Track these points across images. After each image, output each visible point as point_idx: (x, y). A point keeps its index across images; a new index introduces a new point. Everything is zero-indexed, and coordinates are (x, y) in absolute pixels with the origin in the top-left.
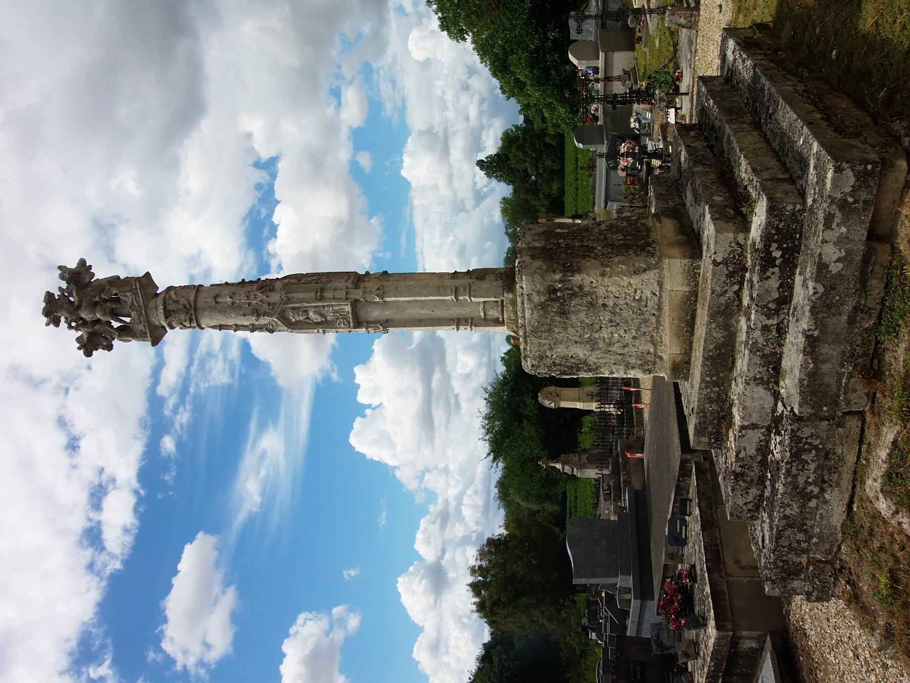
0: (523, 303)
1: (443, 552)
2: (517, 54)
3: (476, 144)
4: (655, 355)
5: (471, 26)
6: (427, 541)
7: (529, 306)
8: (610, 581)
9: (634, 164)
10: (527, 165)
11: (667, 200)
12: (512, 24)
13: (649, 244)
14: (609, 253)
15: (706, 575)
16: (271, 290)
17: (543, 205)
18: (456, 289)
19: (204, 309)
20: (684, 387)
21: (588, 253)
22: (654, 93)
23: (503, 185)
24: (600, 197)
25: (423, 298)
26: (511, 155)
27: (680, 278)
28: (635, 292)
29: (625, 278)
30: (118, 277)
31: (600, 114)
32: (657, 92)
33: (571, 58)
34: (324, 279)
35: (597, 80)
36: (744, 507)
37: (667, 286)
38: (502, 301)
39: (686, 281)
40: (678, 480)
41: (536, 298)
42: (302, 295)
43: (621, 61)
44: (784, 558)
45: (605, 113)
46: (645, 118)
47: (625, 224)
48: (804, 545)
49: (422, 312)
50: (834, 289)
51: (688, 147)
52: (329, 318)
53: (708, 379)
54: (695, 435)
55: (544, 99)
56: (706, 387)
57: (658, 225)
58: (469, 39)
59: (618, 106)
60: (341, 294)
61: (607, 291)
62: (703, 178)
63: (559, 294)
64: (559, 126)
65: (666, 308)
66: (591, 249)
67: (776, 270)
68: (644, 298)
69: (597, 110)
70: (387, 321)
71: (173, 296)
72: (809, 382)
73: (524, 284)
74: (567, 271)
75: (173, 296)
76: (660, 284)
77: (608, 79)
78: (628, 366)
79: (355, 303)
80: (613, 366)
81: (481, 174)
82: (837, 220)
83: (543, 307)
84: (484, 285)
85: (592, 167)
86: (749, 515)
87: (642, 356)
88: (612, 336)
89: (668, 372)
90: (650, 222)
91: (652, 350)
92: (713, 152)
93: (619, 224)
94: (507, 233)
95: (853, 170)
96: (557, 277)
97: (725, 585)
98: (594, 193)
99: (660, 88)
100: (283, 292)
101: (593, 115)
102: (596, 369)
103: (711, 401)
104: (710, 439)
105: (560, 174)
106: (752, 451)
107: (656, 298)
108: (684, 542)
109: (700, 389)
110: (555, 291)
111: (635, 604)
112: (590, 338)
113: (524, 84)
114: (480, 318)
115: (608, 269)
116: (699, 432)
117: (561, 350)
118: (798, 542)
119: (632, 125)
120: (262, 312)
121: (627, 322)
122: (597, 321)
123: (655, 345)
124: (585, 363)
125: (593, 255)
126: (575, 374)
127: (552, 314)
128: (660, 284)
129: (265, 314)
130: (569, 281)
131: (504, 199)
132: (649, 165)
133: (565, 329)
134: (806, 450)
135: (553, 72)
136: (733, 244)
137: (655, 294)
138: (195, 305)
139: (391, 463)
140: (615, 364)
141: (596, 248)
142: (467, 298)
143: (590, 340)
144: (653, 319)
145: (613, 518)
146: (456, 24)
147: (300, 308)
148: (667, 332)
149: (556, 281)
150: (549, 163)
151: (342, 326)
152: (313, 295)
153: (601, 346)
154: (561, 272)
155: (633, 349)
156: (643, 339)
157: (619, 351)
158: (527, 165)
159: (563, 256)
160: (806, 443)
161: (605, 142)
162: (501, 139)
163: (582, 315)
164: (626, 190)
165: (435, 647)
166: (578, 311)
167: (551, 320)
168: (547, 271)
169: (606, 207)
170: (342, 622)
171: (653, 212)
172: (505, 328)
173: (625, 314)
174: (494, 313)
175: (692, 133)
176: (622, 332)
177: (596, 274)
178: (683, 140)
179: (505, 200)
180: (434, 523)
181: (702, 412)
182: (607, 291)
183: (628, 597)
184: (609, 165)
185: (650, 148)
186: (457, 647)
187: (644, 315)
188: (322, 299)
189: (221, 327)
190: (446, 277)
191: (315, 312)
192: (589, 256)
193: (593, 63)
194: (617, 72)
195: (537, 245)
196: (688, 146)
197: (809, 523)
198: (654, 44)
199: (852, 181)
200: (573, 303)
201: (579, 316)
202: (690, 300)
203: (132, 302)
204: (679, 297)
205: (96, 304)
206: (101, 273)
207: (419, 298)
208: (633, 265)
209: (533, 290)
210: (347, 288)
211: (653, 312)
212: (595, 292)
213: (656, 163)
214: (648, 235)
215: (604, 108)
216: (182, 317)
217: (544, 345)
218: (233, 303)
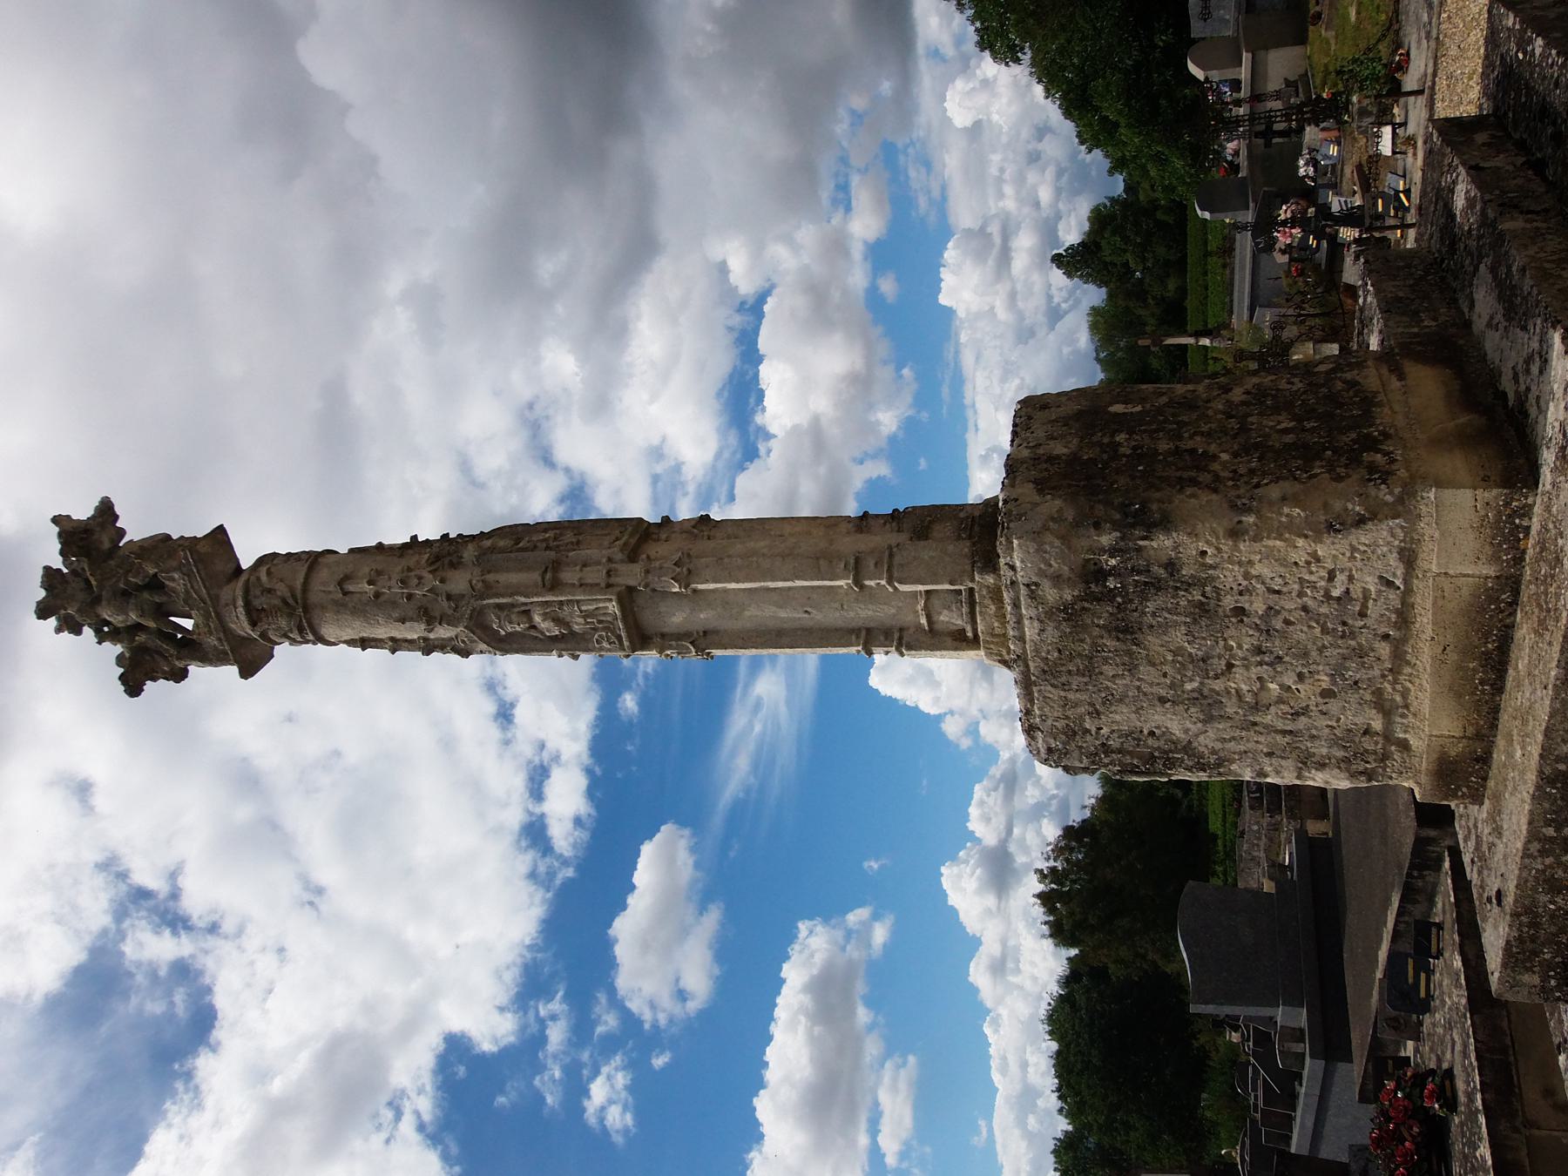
0: (1016, 605)
1: (1009, 831)
2: (1104, 78)
3: (1049, 230)
4: (1388, 736)
5: (1026, 35)
6: (987, 819)
7: (1033, 612)
8: (1266, 1012)
9: (1304, 239)
10: (1129, 256)
11: (1416, 313)
12: (1095, 28)
13: (1371, 444)
14: (1252, 472)
15: (1482, 1120)
16: (454, 566)
17: (1153, 315)
18: (857, 561)
19: (323, 608)
20: (1470, 818)
21: (1192, 471)
22: (1348, 101)
23: (1091, 287)
24: (1241, 301)
25: (780, 584)
26: (1103, 243)
27: (1469, 542)
28: (1331, 576)
29: (1300, 542)
30: (168, 537)
31: (1243, 160)
32: (1355, 99)
33: (1193, 68)
34: (569, 537)
35: (1238, 103)
37: (1430, 561)
38: (971, 590)
39: (1488, 550)
40: (1409, 875)
41: (1050, 594)
42: (514, 578)
43: (1281, 64)
45: (1250, 156)
46: (1326, 157)
47: (1299, 385)
49: (783, 614)
51: (1475, 170)
52: (576, 628)
53: (1550, 832)
54: (1505, 965)
55: (1149, 147)
56: (1543, 853)
57: (1395, 384)
58: (1027, 57)
59: (1275, 145)
60: (595, 575)
61: (1247, 576)
62: (1532, 251)
63: (1111, 583)
64: (1173, 189)
65: (1424, 621)
66: (1201, 461)
68: (1356, 592)
69: (1236, 153)
70: (705, 633)
71: (264, 578)
73: (1017, 557)
74: (1133, 526)
75: (264, 578)
76: (1409, 558)
77: (1256, 97)
78: (1306, 761)
79: (628, 598)
80: (1266, 760)
81: (1057, 276)
83: (1069, 614)
84: (926, 551)
85: (1228, 250)
87: (1345, 739)
88: (1263, 688)
89: (1424, 779)
90: (1371, 378)
91: (1377, 725)
92: (1544, 179)
93: (1283, 385)
94: (1097, 359)
96: (1106, 540)
97: (1524, 1152)
98: (1231, 294)
99: (1361, 89)
100: (477, 571)
101: (1231, 163)
102: (1219, 765)
105: (1181, 265)
107: (1394, 598)
108: (1425, 1006)
109: (1526, 854)
110: (1101, 575)
111: (1311, 1068)
112: (1199, 691)
113: (1116, 125)
114: (919, 627)
115: (1251, 519)
116: (1516, 956)
117: (1122, 718)
119: (1302, 172)
120: (437, 614)
121: (1306, 655)
122: (1219, 649)
124: (1188, 748)
125: (1205, 478)
126: (1162, 774)
127: (1096, 632)
128: (1409, 558)
129: (443, 619)
130: (1139, 550)
131: (1093, 308)
132: (1333, 239)
133: (1132, 669)
135: (1163, 102)
137: (1390, 584)
138: (305, 599)
139: (927, 706)
140: (1270, 755)
141: (1215, 457)
142: (883, 582)
143: (1199, 697)
144: (1384, 649)
145: (1268, 887)
146: (1002, 34)
147: (513, 605)
148: (1426, 681)
149: (1103, 551)
150: (1161, 251)
151: (605, 644)
152: (535, 576)
153: (1230, 710)
154: (1116, 526)
155: (1323, 722)
156: (1353, 698)
157: (1280, 725)
158: (1129, 256)
159: (1123, 481)
161: (1251, 205)
162: (1089, 219)
163: (1178, 637)
164: (1289, 285)
165: (998, 968)
166: (1165, 627)
167: (1094, 644)
168: (1077, 524)
169: (1251, 318)
170: (865, 931)
171: (1374, 343)
172: (982, 653)
173: (1300, 634)
174: (951, 618)
175: (1481, 138)
176: (1289, 679)
177: (1214, 532)
178: (1459, 153)
179: (1095, 311)
180: (995, 789)
181: (1526, 914)
182: (1247, 576)
183: (1298, 1048)
184: (1257, 244)
185: (1335, 208)
186: (1033, 964)
187: (1359, 642)
188: (555, 586)
189: (364, 643)
190: (844, 527)
191: (545, 616)
192: (1194, 482)
193: (1230, 74)
194: (1274, 84)
195: (1059, 449)
196: (1471, 168)
198: (1346, 17)
200: (1151, 606)
201: (1174, 639)
202: (1497, 601)
203: (187, 592)
204: (1465, 592)
205: (126, 594)
206: (136, 526)
207: (771, 585)
208: (1326, 506)
209: (1041, 573)
210: (610, 560)
211: (1383, 630)
212: (1213, 579)
213: (1347, 234)
214: (1367, 416)
215: (1249, 147)
216: (283, 623)
217: (1076, 705)
218: (377, 595)
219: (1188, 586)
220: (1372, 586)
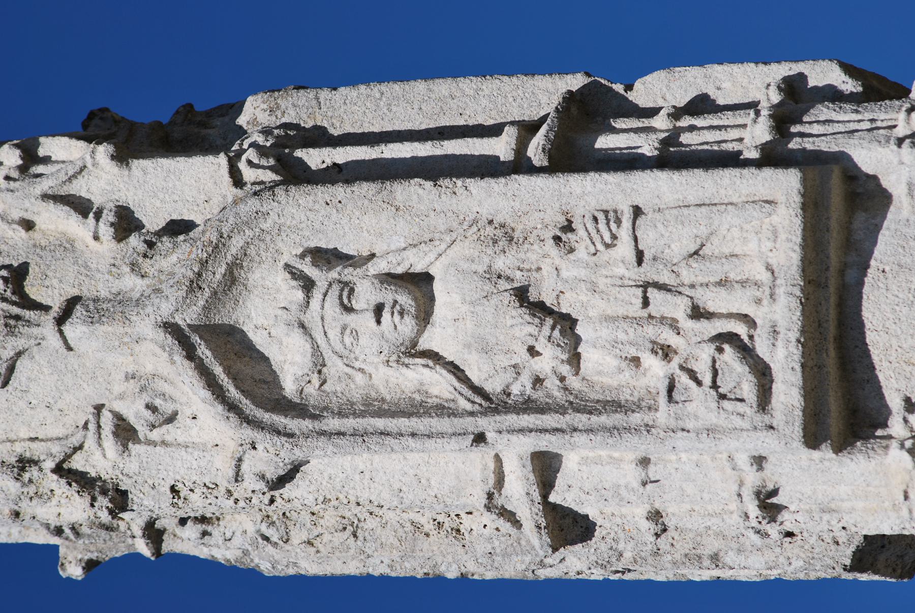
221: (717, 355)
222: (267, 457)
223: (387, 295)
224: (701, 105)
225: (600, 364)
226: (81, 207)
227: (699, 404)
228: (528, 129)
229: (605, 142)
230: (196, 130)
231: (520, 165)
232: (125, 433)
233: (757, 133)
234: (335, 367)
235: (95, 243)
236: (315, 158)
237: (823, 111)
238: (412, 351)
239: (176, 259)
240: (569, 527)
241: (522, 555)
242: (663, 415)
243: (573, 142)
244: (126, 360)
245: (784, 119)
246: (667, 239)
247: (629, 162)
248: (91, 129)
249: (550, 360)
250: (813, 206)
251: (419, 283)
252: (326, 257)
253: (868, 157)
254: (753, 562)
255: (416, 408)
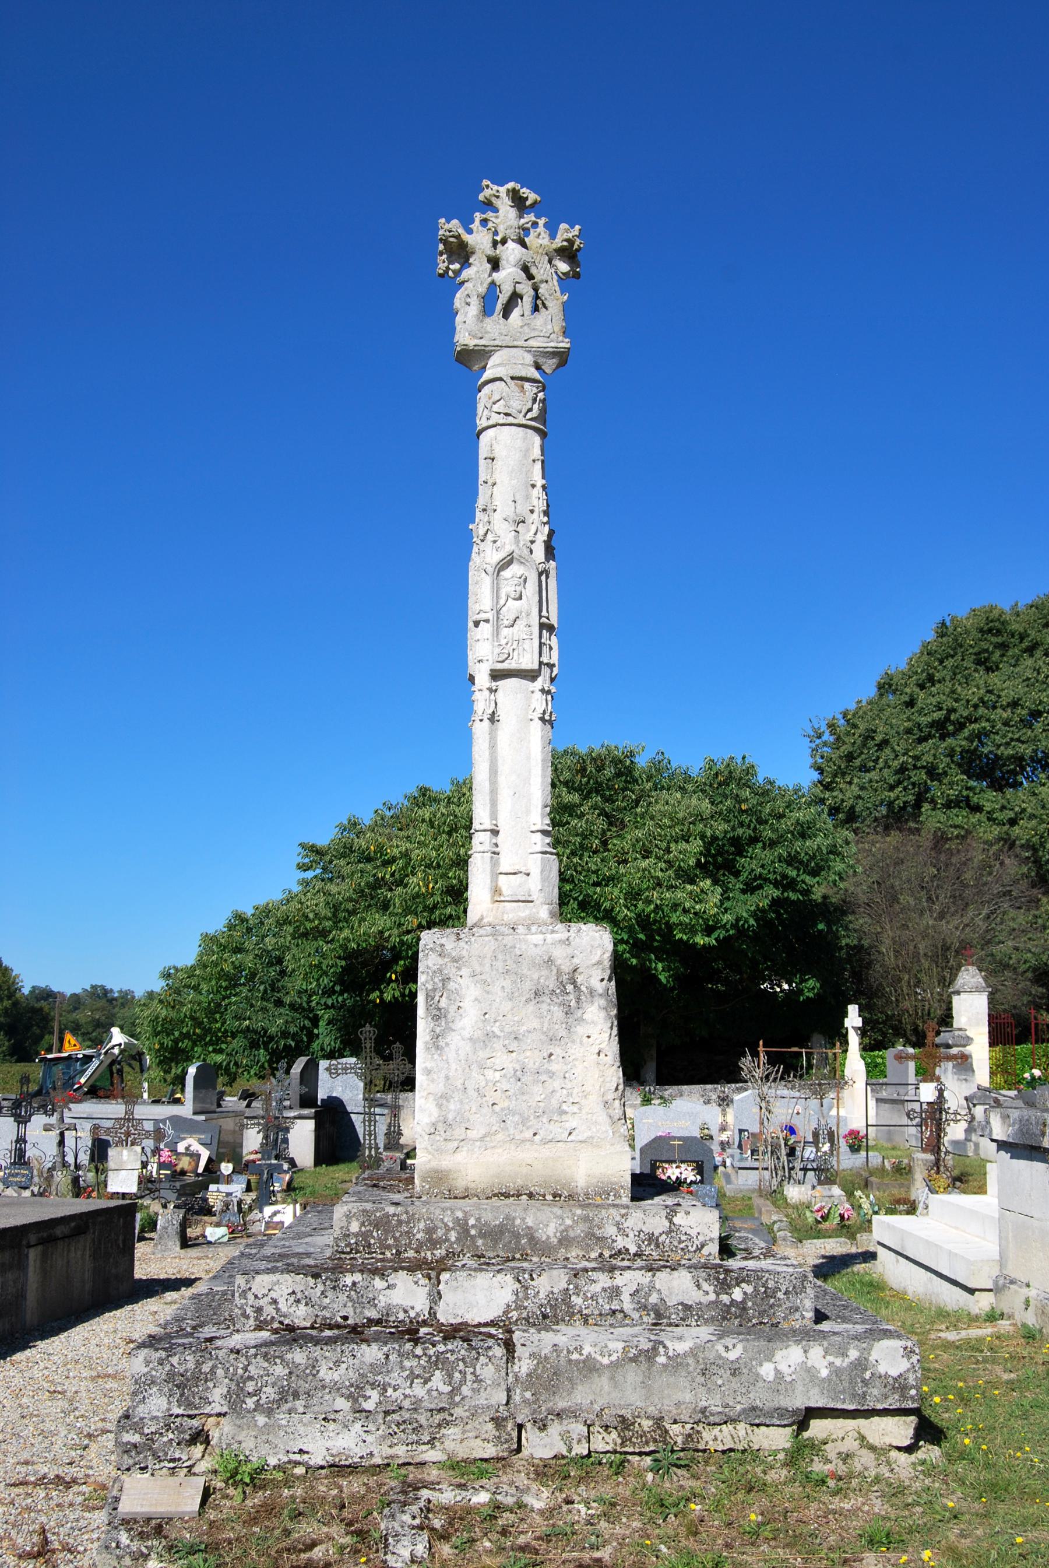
36: (268, 1299)
44: (220, 1372)
48: (250, 1403)
50: (733, 1374)
67: (712, 1297)
72: (577, 1361)
80: (443, 1075)
82: (838, 1362)
86: (249, 1310)
95: (908, 1370)
102: (438, 1048)
103: (430, 1231)
104: (356, 1235)
106: (382, 1301)
118: (257, 1393)
123: (482, 1139)
127: (535, 976)
134: (450, 1376)
136: (701, 1238)
140: (447, 1078)
157: (471, 1086)
160: (463, 1373)
173: (537, 1089)
197: (299, 1405)
199: (894, 1373)
201: (531, 1019)
219: (568, 1029)
220: (573, 1123)
221: (433, 1305)
222: (490, 570)
223: (518, 593)
224: (551, 648)
225: (505, 632)
226: (535, 534)
227: (497, 650)
228: (548, 618)
229: (544, 632)
230: (550, 552)
231: (541, 617)
232: (495, 542)
233: (545, 660)
234: (506, 582)
235: (529, 536)
236: (543, 578)
237: (549, 671)
238: (508, 597)
239: (526, 552)
240: (477, 624)
241: (472, 617)
242: (496, 644)
243: (546, 627)
244: (508, 545)
245: (548, 664)
246: (527, 645)
247: (540, 637)
248: (551, 533)
249: (506, 623)
250: (532, 671)
251: (520, 598)
252: (525, 581)
253: (540, 679)
254: (471, 657)
255: (498, 597)
